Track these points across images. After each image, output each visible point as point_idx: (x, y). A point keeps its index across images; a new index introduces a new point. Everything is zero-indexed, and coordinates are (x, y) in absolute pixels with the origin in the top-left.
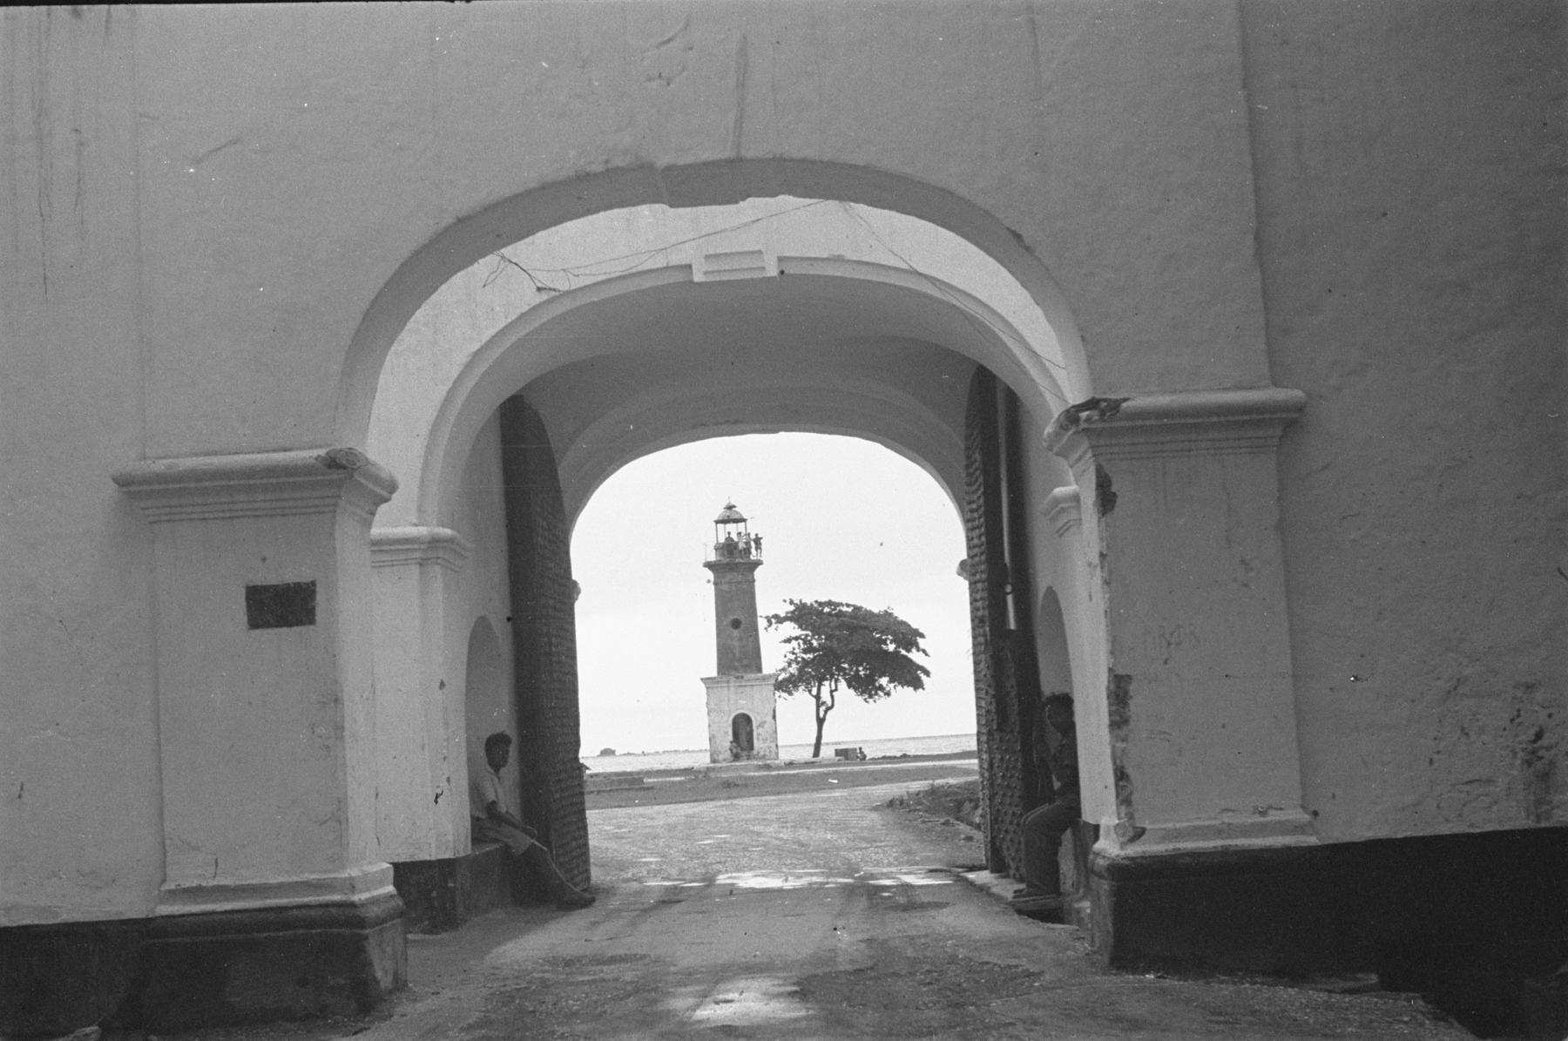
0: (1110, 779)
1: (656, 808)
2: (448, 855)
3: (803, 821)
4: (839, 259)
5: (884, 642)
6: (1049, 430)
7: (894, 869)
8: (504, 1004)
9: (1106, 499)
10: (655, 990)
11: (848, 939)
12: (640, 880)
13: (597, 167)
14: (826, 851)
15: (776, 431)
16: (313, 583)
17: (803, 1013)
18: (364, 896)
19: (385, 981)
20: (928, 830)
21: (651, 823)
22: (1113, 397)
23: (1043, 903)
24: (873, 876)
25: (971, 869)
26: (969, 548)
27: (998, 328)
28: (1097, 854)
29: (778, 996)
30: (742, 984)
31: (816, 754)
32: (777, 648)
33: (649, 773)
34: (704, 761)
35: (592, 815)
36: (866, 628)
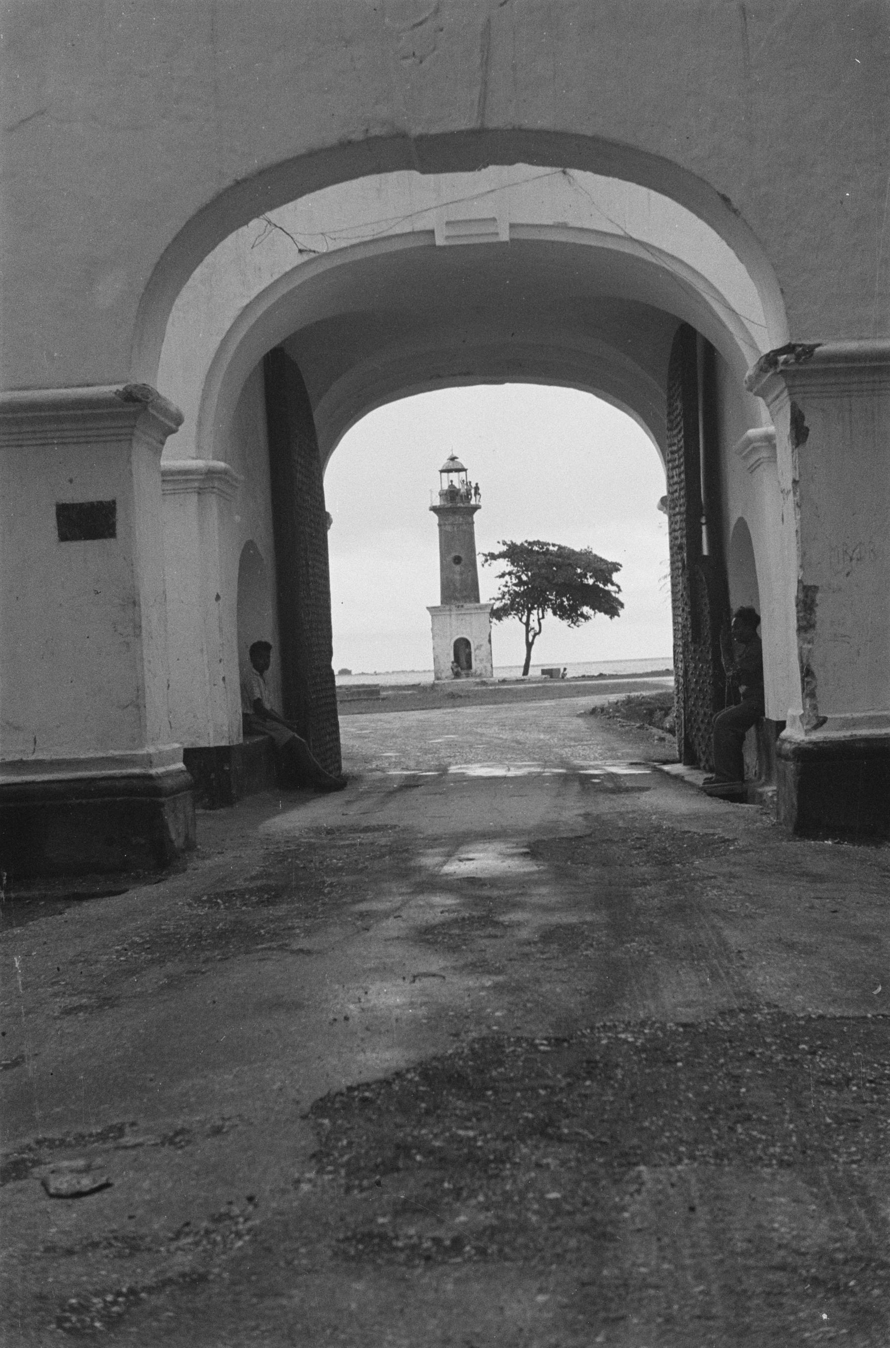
0: (797, 675)
1: (393, 714)
2: (224, 743)
3: (518, 725)
4: (564, 227)
5: (585, 576)
6: (750, 372)
7: (599, 763)
8: (281, 862)
9: (800, 433)
10: (407, 851)
11: (571, 812)
12: (383, 770)
13: (358, 136)
14: (539, 747)
15: (502, 382)
16: (114, 502)
17: (535, 868)
18: (161, 770)
19: (179, 842)
20: (627, 732)
21: (388, 726)
22: (807, 342)
23: (730, 784)
24: (582, 768)
25: (666, 762)
26: (670, 485)
27: (700, 287)
28: (784, 741)
29: (512, 856)
30: (480, 847)
31: (526, 672)
32: (493, 581)
33: (385, 688)
34: (430, 679)
35: (342, 719)
36: (570, 564)
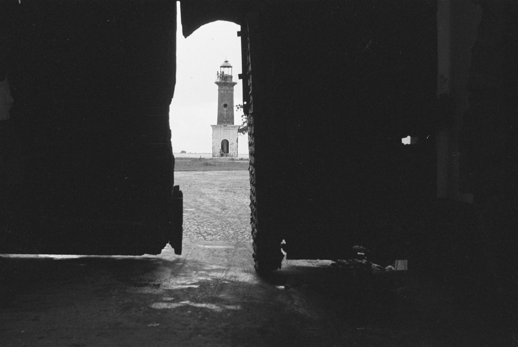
35: (175, 173)
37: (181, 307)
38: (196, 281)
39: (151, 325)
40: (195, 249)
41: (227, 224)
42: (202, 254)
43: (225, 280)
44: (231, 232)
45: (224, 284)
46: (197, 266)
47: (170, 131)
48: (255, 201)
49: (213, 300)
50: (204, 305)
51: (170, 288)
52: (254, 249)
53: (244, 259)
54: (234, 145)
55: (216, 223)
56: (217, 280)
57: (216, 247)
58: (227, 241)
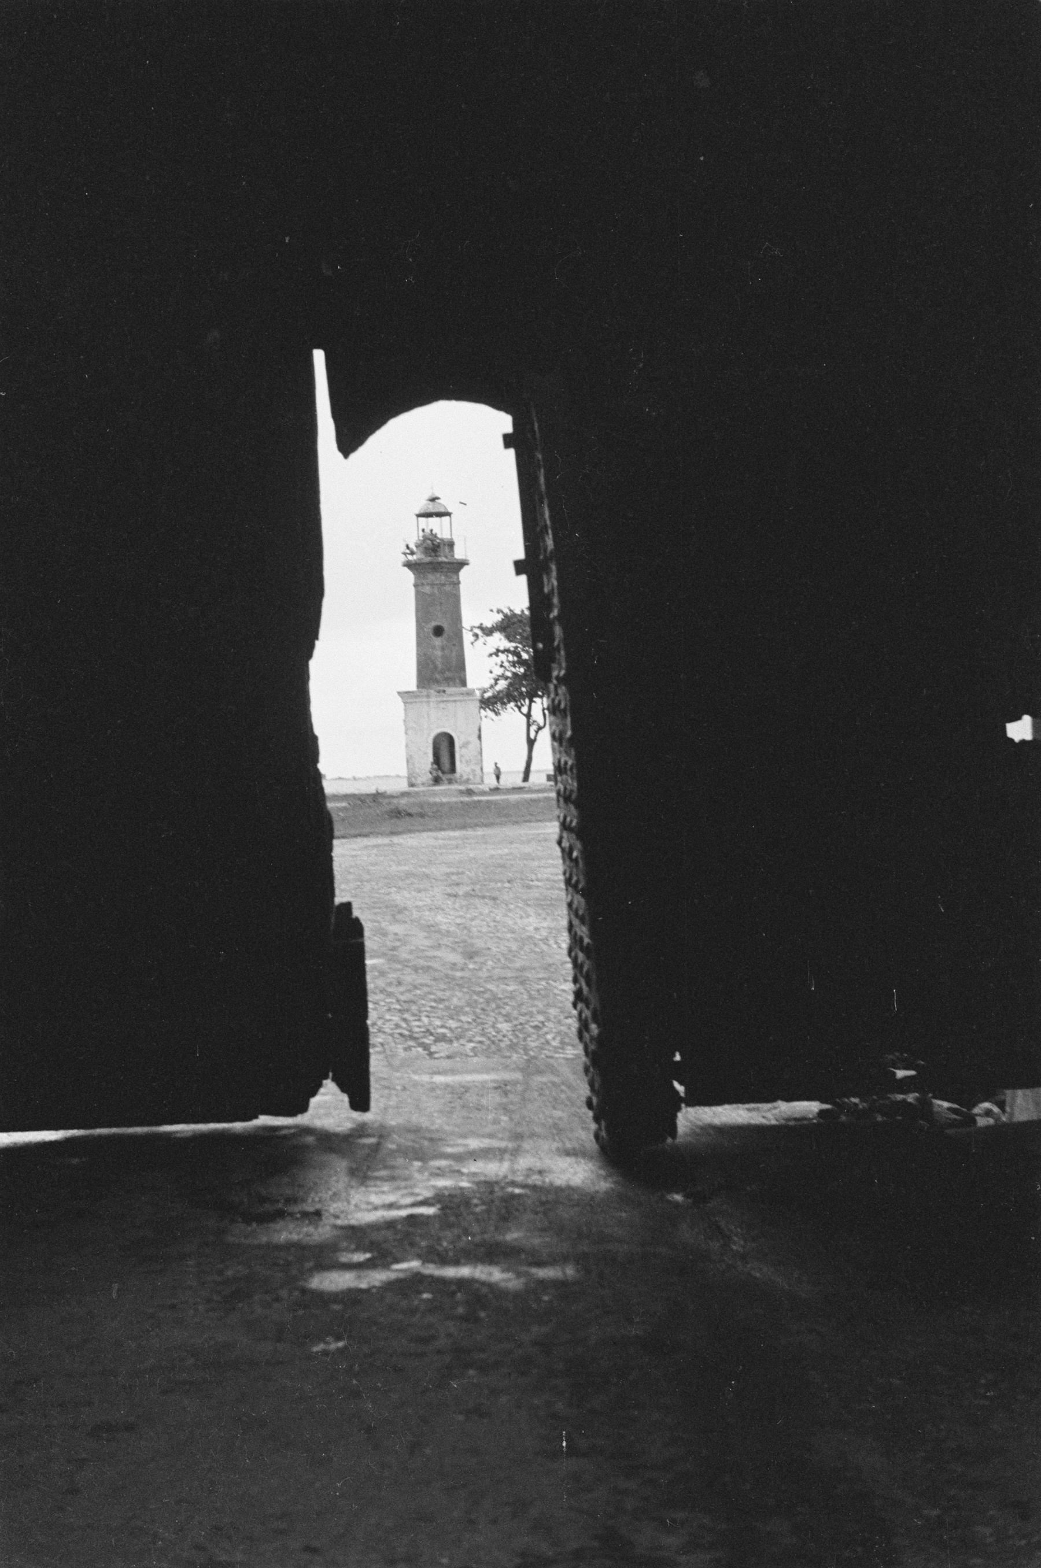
37: (398, 1281)
38: (428, 1194)
39: (321, 1347)
40: (404, 1089)
41: (488, 1002)
42: (432, 1105)
43: (513, 1184)
44: (504, 1026)
45: (513, 1196)
46: (423, 1147)
47: (315, 739)
48: (586, 940)
49: (491, 1253)
50: (465, 1271)
51: (353, 1222)
52: (591, 1084)
53: (558, 1113)
54: (471, 747)
55: (455, 1001)
56: (489, 1185)
57: (469, 1078)
58: (496, 1058)
